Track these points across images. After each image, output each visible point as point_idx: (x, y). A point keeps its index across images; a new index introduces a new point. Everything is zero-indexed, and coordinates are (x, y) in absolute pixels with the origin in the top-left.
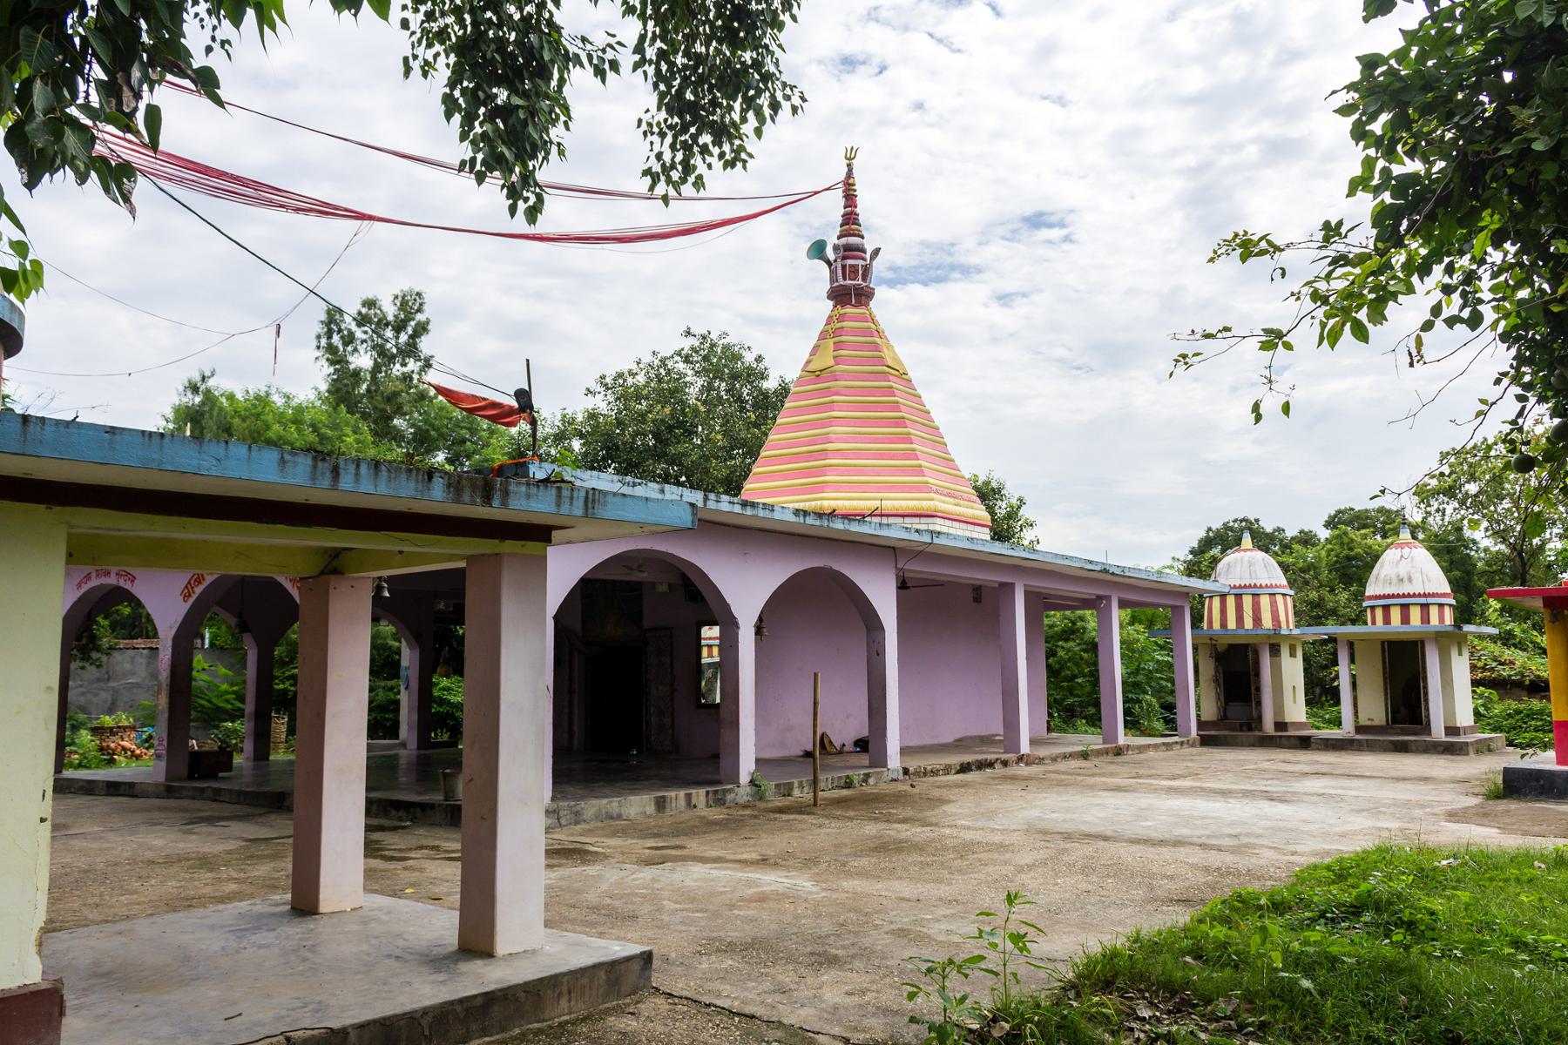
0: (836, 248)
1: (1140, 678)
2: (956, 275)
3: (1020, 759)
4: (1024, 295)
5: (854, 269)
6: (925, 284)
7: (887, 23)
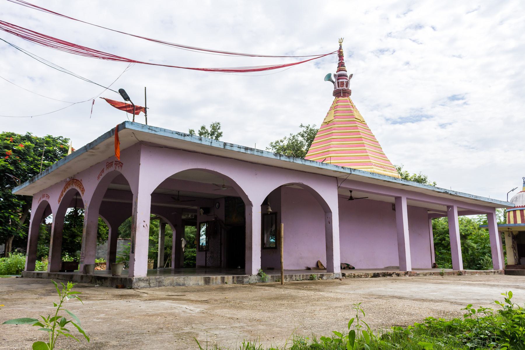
0: (335, 75)
1: (486, 250)
2: (424, 119)
3: (407, 273)
4: (450, 124)
5: (342, 83)
6: (413, 123)
7: (394, 37)
